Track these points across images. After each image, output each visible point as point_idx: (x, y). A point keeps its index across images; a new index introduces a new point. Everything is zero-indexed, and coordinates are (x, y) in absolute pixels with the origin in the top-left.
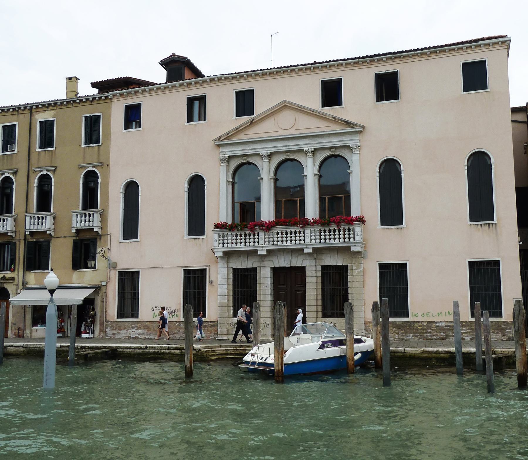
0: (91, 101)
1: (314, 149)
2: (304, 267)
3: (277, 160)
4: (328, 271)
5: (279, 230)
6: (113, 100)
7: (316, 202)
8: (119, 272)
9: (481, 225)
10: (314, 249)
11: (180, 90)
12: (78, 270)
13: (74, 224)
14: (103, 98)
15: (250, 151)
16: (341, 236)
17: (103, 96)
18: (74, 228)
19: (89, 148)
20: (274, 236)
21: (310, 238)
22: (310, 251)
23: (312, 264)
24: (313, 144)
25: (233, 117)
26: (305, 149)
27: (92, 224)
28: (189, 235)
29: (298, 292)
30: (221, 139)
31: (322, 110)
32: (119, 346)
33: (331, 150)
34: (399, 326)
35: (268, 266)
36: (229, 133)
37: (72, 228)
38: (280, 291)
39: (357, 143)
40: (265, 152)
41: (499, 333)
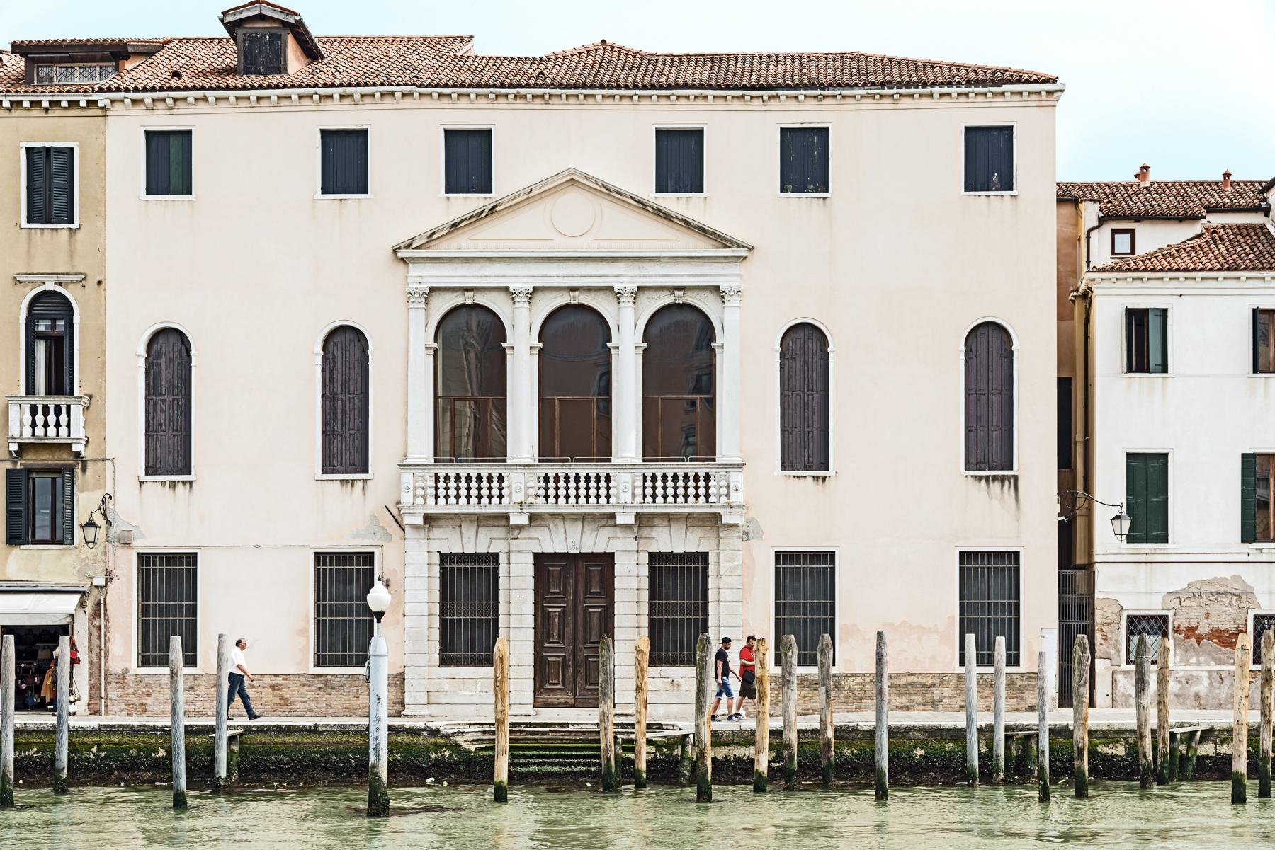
0: (46, 110)
1: (638, 287)
2: (612, 555)
3: (546, 306)
4: (693, 566)
5: (494, 471)
6: (109, 113)
7: (637, 408)
8: (140, 555)
9: (987, 478)
10: (638, 517)
11: (298, 109)
12: (22, 547)
13: (14, 430)
14: (83, 104)
15: (484, 279)
16: (482, 492)
17: (82, 98)
18: (13, 441)
19: (42, 234)
20: (721, 484)
21: (523, 492)
22: (630, 520)
23: (629, 548)
24: (635, 276)
25: (439, 193)
26: (617, 287)
27: (66, 433)
28: (324, 472)
29: (591, 610)
30: (414, 246)
31: (656, 198)
32: (205, 723)
33: (676, 293)
34: (815, 684)
35: (528, 551)
36: (433, 234)
37: (10, 441)
38: (591, 607)
39: (736, 285)
40: (521, 285)
41: (629, 783)
